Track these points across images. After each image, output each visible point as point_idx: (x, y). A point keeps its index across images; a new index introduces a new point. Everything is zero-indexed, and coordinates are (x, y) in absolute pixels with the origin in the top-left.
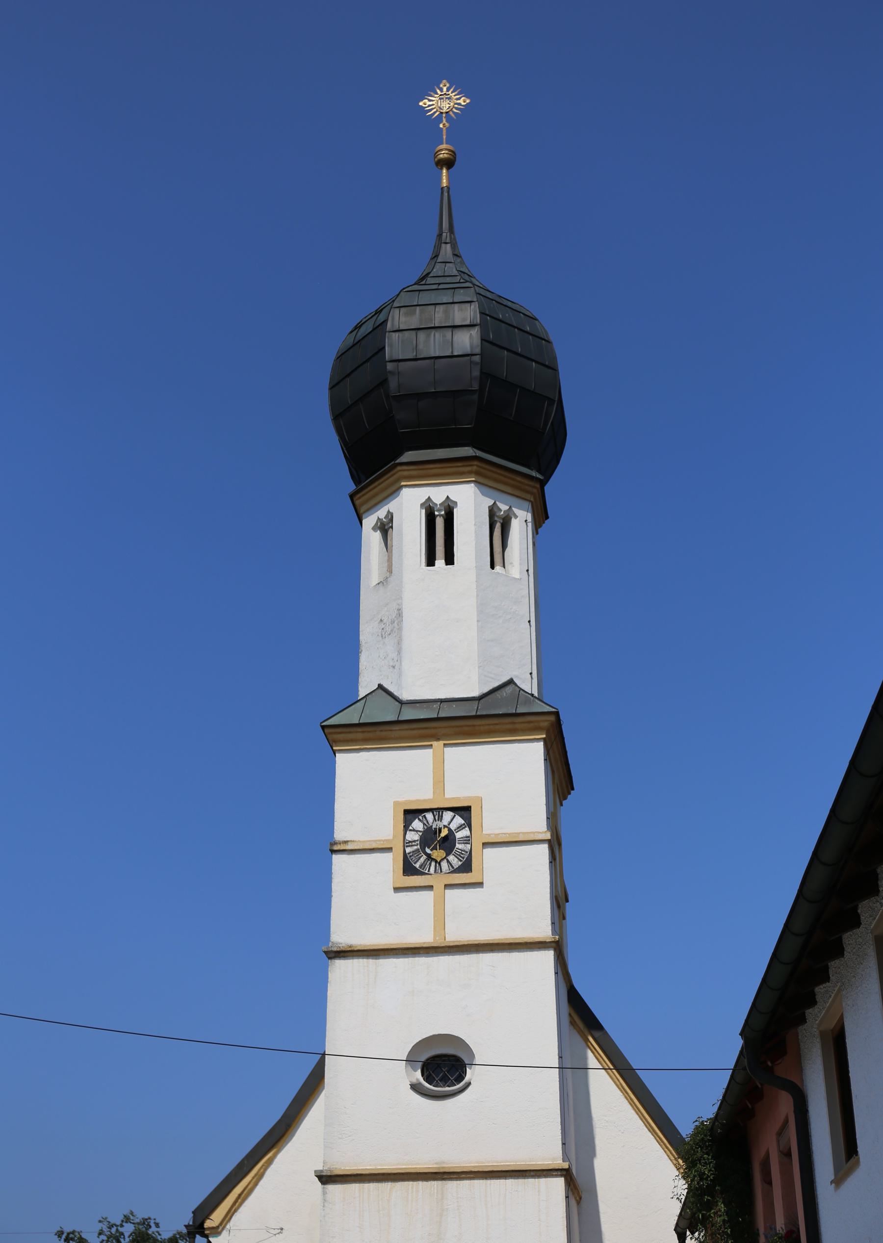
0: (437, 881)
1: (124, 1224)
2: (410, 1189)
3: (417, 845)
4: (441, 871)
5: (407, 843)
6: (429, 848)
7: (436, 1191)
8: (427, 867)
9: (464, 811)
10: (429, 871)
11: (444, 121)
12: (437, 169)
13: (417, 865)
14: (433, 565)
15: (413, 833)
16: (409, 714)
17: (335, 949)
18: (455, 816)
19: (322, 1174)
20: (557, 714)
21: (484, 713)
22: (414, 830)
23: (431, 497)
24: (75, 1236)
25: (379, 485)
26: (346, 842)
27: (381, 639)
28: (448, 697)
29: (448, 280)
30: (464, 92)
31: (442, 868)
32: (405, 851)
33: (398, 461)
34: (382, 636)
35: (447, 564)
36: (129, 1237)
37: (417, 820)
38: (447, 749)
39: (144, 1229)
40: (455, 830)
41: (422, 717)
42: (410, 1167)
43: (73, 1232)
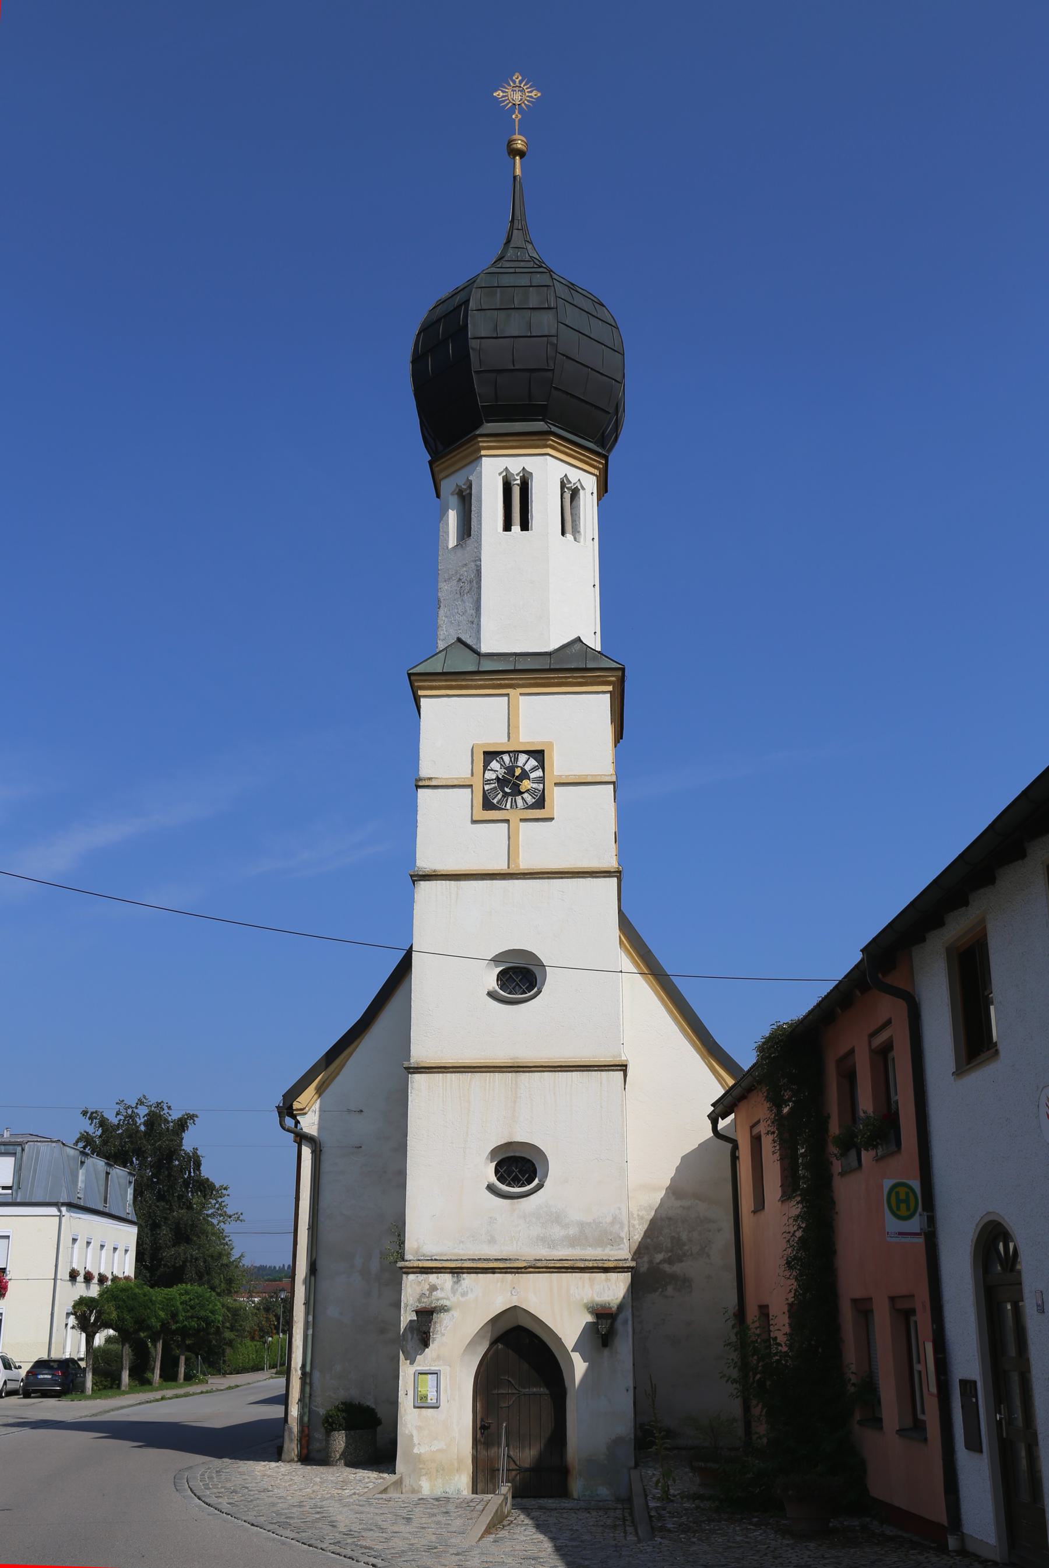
0: (513, 815)
1: (138, 1106)
2: (488, 1079)
3: (495, 783)
4: (517, 807)
6: (507, 788)
7: (510, 1082)
8: (504, 803)
9: (538, 755)
10: (505, 806)
13: (495, 801)
15: (491, 772)
16: (487, 665)
17: (421, 873)
18: (529, 758)
20: (623, 670)
21: (558, 667)
22: (492, 770)
23: (508, 468)
24: (98, 1115)
25: (459, 453)
26: (430, 779)
28: (523, 651)
29: (522, 264)
31: (518, 804)
32: (484, 788)
33: (478, 432)
35: (522, 530)
36: (144, 1117)
37: (495, 761)
38: (521, 698)
39: (158, 1111)
41: (501, 669)
42: (488, 1061)
43: (96, 1112)
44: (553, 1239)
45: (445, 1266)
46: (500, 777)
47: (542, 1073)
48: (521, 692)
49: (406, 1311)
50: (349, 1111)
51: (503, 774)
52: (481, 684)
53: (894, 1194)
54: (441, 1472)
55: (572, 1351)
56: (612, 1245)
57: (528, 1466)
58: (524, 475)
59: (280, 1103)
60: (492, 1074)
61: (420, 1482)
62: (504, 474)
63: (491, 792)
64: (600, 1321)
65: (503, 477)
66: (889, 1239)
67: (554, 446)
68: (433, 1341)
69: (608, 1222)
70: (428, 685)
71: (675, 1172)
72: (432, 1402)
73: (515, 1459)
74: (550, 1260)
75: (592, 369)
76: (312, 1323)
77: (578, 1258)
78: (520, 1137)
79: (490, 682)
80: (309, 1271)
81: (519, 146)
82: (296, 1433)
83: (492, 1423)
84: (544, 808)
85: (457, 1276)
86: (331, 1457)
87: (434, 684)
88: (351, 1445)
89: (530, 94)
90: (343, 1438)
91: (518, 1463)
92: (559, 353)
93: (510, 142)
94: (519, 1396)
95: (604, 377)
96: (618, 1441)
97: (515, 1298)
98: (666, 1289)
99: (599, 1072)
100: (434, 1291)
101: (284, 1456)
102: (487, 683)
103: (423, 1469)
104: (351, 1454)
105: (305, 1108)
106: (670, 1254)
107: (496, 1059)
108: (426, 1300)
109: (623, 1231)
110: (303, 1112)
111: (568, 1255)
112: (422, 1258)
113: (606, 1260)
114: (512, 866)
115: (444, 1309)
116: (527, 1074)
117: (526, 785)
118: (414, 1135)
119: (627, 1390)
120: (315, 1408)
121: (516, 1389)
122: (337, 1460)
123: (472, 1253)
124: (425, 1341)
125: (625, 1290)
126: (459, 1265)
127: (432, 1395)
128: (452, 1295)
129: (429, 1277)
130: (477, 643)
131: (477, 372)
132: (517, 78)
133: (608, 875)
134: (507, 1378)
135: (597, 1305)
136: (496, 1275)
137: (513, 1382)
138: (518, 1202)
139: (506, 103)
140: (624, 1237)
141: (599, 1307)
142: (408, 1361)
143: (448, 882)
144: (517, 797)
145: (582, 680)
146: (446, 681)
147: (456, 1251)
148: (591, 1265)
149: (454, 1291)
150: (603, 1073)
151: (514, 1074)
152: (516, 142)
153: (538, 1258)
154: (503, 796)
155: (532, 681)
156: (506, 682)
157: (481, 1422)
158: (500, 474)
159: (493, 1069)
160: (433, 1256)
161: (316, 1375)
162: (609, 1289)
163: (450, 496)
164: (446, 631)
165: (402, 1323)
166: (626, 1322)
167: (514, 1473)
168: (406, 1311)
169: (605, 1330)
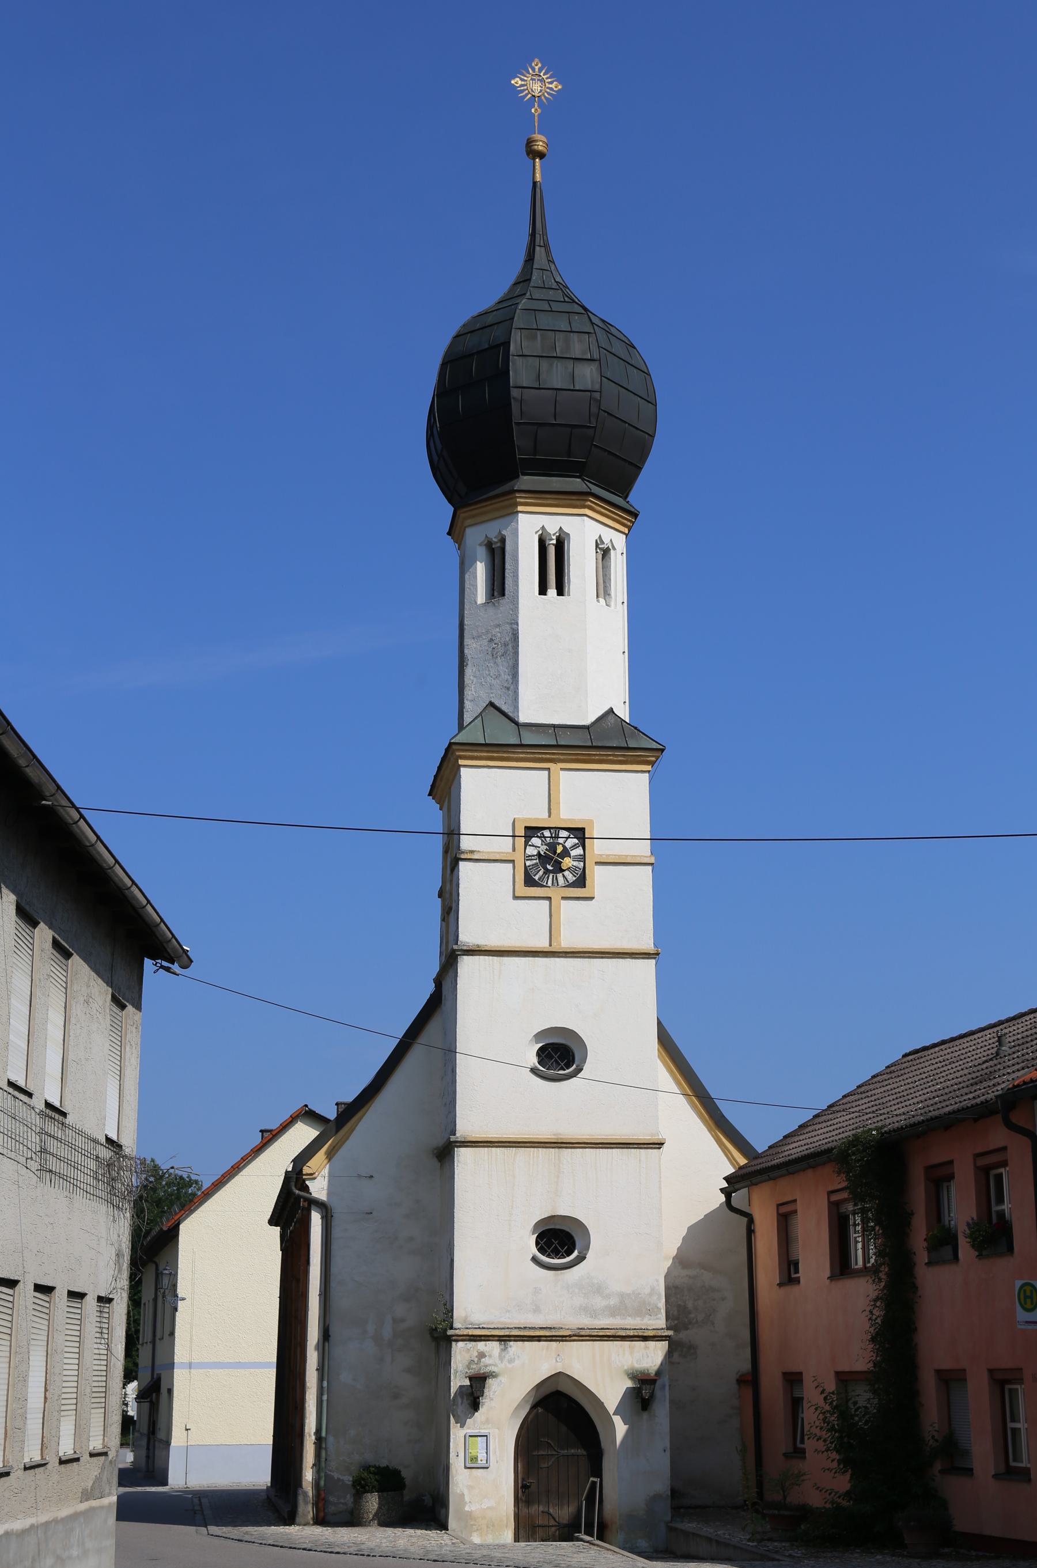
3: (536, 859)
4: (558, 885)
5: (527, 857)
6: (549, 865)
7: (553, 1157)
9: (579, 833)
10: (547, 883)
11: (536, 106)
12: (528, 158)
13: (536, 878)
14: (545, 594)
15: (532, 847)
16: (529, 738)
17: (465, 948)
19: (457, 1140)
22: (533, 846)
25: (491, 504)
26: (472, 852)
27: (491, 658)
28: (561, 723)
30: (556, 76)
31: (559, 882)
32: (525, 864)
34: (493, 656)
35: (558, 595)
38: (562, 773)
40: (570, 848)
41: (543, 743)
42: (531, 1136)
44: (594, 1309)
45: (493, 1334)
46: (542, 853)
47: (584, 1149)
48: (562, 767)
49: (455, 1377)
50: (359, 1176)
51: (544, 851)
52: (522, 757)
53: (1022, 1291)
54: (491, 1527)
55: (613, 1414)
56: (650, 1315)
57: (567, 1523)
58: (560, 535)
59: (288, 1166)
60: (536, 1149)
61: (472, 1538)
62: (540, 532)
63: (532, 868)
64: (644, 1387)
65: (539, 535)
66: (1019, 1327)
67: (591, 506)
68: (482, 1406)
69: (646, 1293)
70: (470, 755)
71: (681, 1241)
72: (482, 1462)
73: (555, 1516)
74: (592, 1329)
75: (629, 424)
76: (326, 1388)
77: (618, 1327)
78: (563, 1211)
79: (532, 756)
80: (322, 1337)
81: (540, 148)
82: (311, 1497)
83: (534, 1482)
84: (585, 887)
85: (505, 1344)
86: (363, 1518)
87: (476, 754)
88: (384, 1506)
89: (550, 86)
90: (376, 1499)
91: (557, 1520)
92: (602, 410)
93: (530, 143)
94: (558, 1458)
95: (639, 431)
96: (655, 1498)
97: (559, 1365)
98: (673, 1356)
99: (638, 1150)
100: (482, 1358)
101: (298, 1520)
102: (529, 756)
103: (475, 1525)
104: (385, 1515)
105: (314, 1173)
106: (676, 1322)
107: (539, 1135)
108: (474, 1366)
109: (660, 1302)
110: (312, 1176)
111: (609, 1325)
112: (470, 1326)
113: (644, 1329)
114: (554, 944)
115: (493, 1375)
116: (570, 1150)
117: (567, 862)
118: (461, 1208)
119: (665, 1451)
120: (330, 1473)
121: (555, 1450)
122: (370, 1520)
123: (517, 1321)
124: (475, 1406)
125: (662, 1357)
126: (507, 1333)
127: (482, 1456)
128: (500, 1362)
129: (477, 1345)
130: (514, 712)
131: (518, 424)
132: (537, 65)
133: (647, 956)
134: (546, 1440)
135: (636, 1371)
136: (541, 1343)
137: (552, 1444)
138: (561, 1273)
139: (524, 94)
140: (662, 1307)
141: (638, 1373)
142: (459, 1425)
143: (491, 957)
144: (558, 875)
145: (623, 759)
146: (488, 752)
147: (503, 1320)
148: (632, 1334)
149: (501, 1358)
150: (642, 1151)
151: (557, 1150)
152: (538, 143)
153: (580, 1327)
154: (544, 873)
155: (574, 757)
156: (548, 756)
157: (522, 1482)
158: (536, 533)
159: (537, 1145)
160: (480, 1324)
161: (331, 1439)
162: (648, 1357)
163: (478, 547)
164: (476, 692)
165: (452, 1388)
166: (663, 1387)
167: (553, 1529)
168: (455, 1377)
169: (648, 1394)
